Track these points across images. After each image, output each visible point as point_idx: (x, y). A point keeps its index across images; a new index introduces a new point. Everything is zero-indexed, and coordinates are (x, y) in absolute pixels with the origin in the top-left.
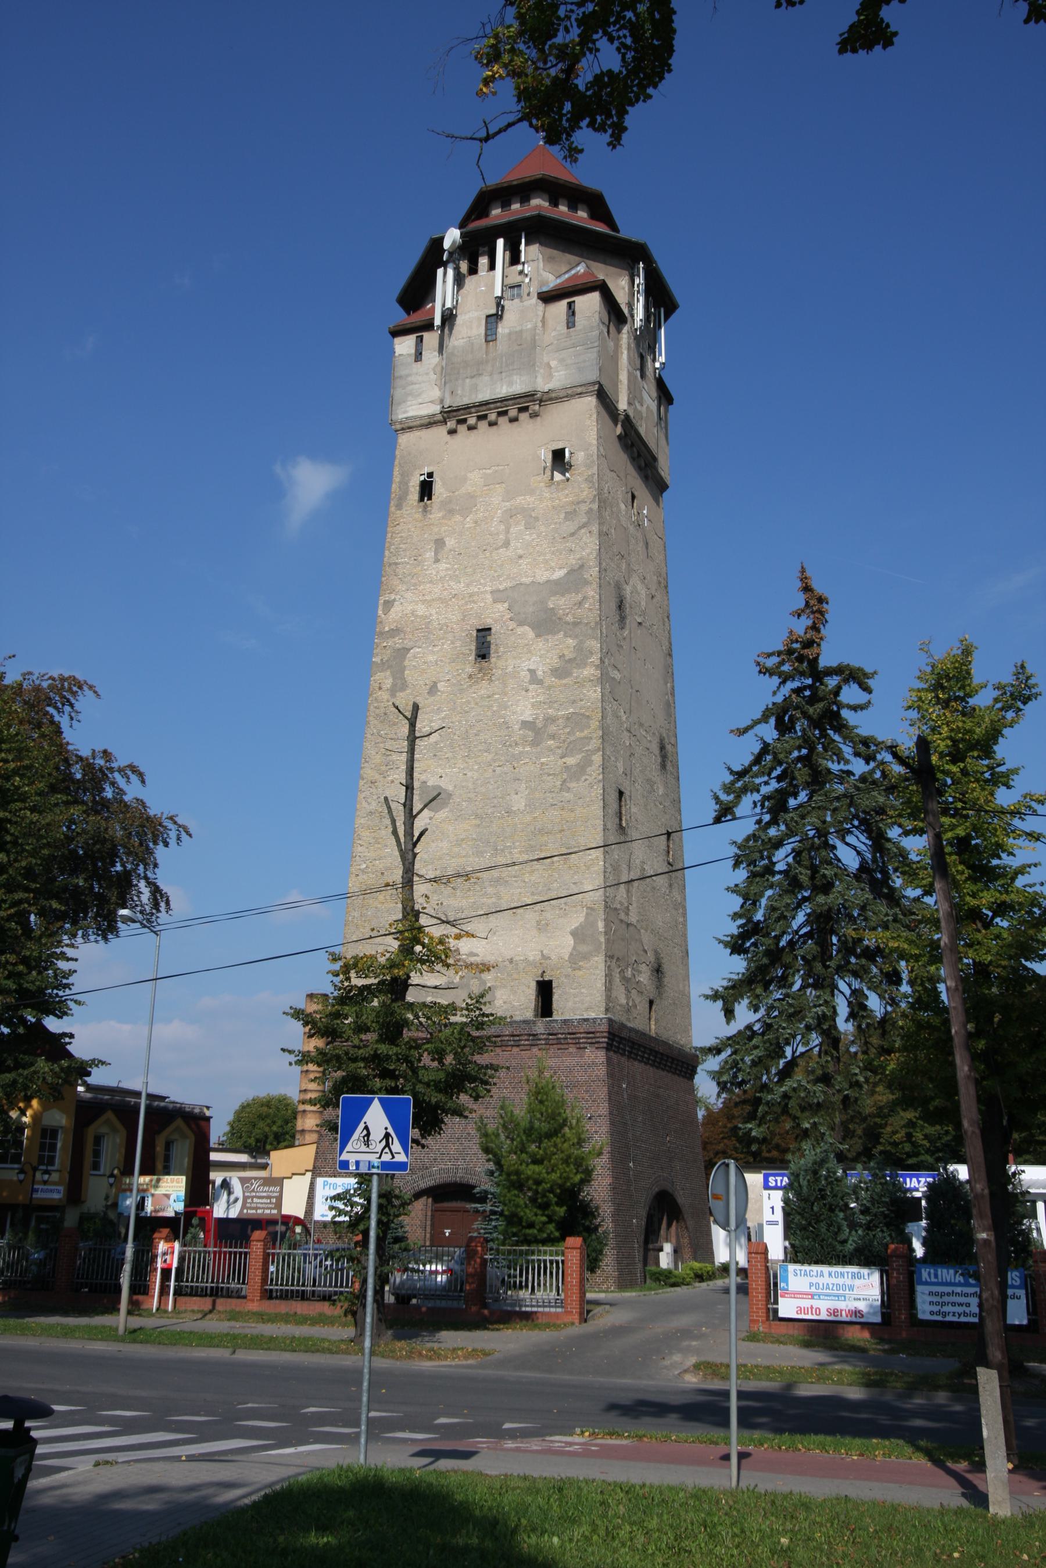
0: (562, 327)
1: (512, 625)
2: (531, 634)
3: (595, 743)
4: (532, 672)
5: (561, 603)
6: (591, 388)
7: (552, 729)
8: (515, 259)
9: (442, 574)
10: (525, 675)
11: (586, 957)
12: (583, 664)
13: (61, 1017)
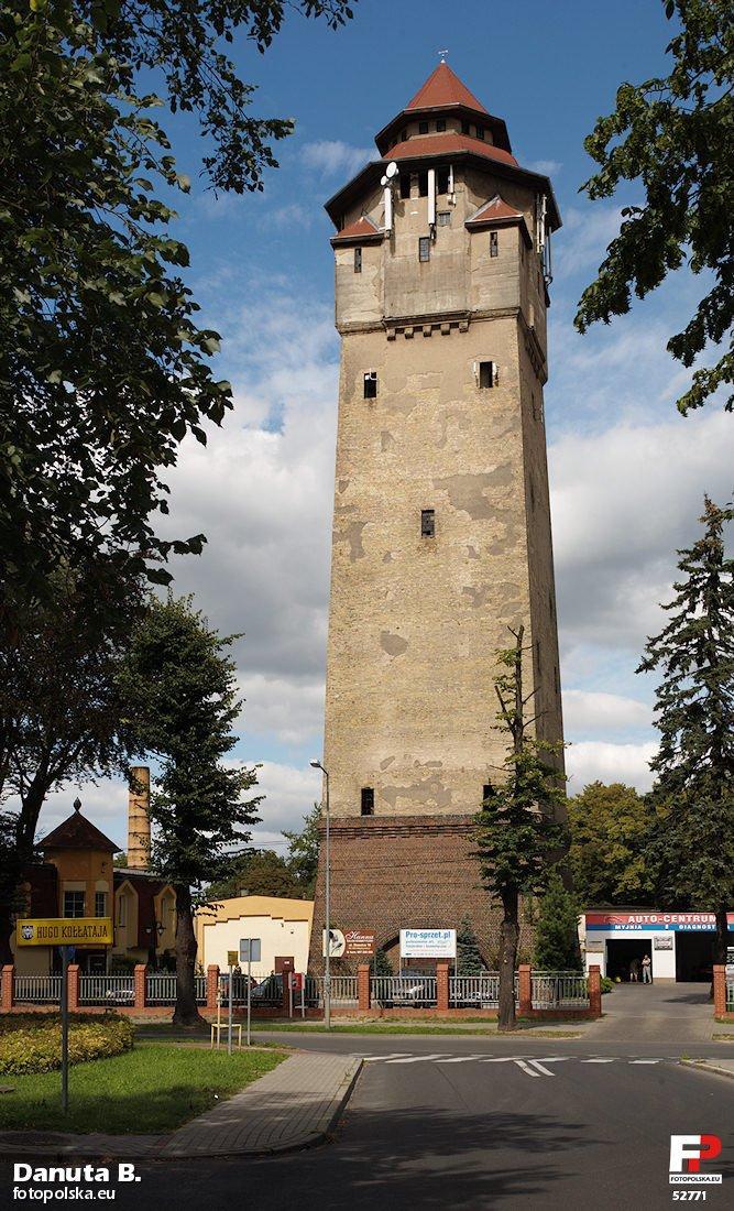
0: (486, 255)
4: (471, 548)
5: (492, 493)
7: (489, 594)
8: (442, 188)
9: (390, 461)
12: (513, 544)
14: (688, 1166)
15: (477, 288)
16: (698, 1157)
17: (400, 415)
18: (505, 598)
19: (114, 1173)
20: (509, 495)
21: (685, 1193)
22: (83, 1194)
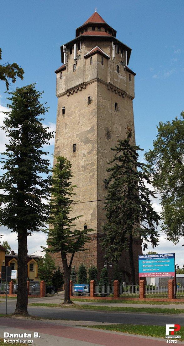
0: (89, 65)
1: (80, 142)
2: (84, 144)
3: (96, 169)
4: (84, 153)
5: (89, 136)
6: (96, 80)
7: (88, 167)
8: (78, 49)
9: (67, 132)
10: (82, 154)
11: (93, 220)
12: (93, 151)
13: (79, 31)
14: (171, 333)
15: (87, 75)
16: (174, 330)
17: (70, 117)
18: (91, 167)
19: (32, 335)
20: (93, 135)
21: (170, 341)
22: (24, 341)
